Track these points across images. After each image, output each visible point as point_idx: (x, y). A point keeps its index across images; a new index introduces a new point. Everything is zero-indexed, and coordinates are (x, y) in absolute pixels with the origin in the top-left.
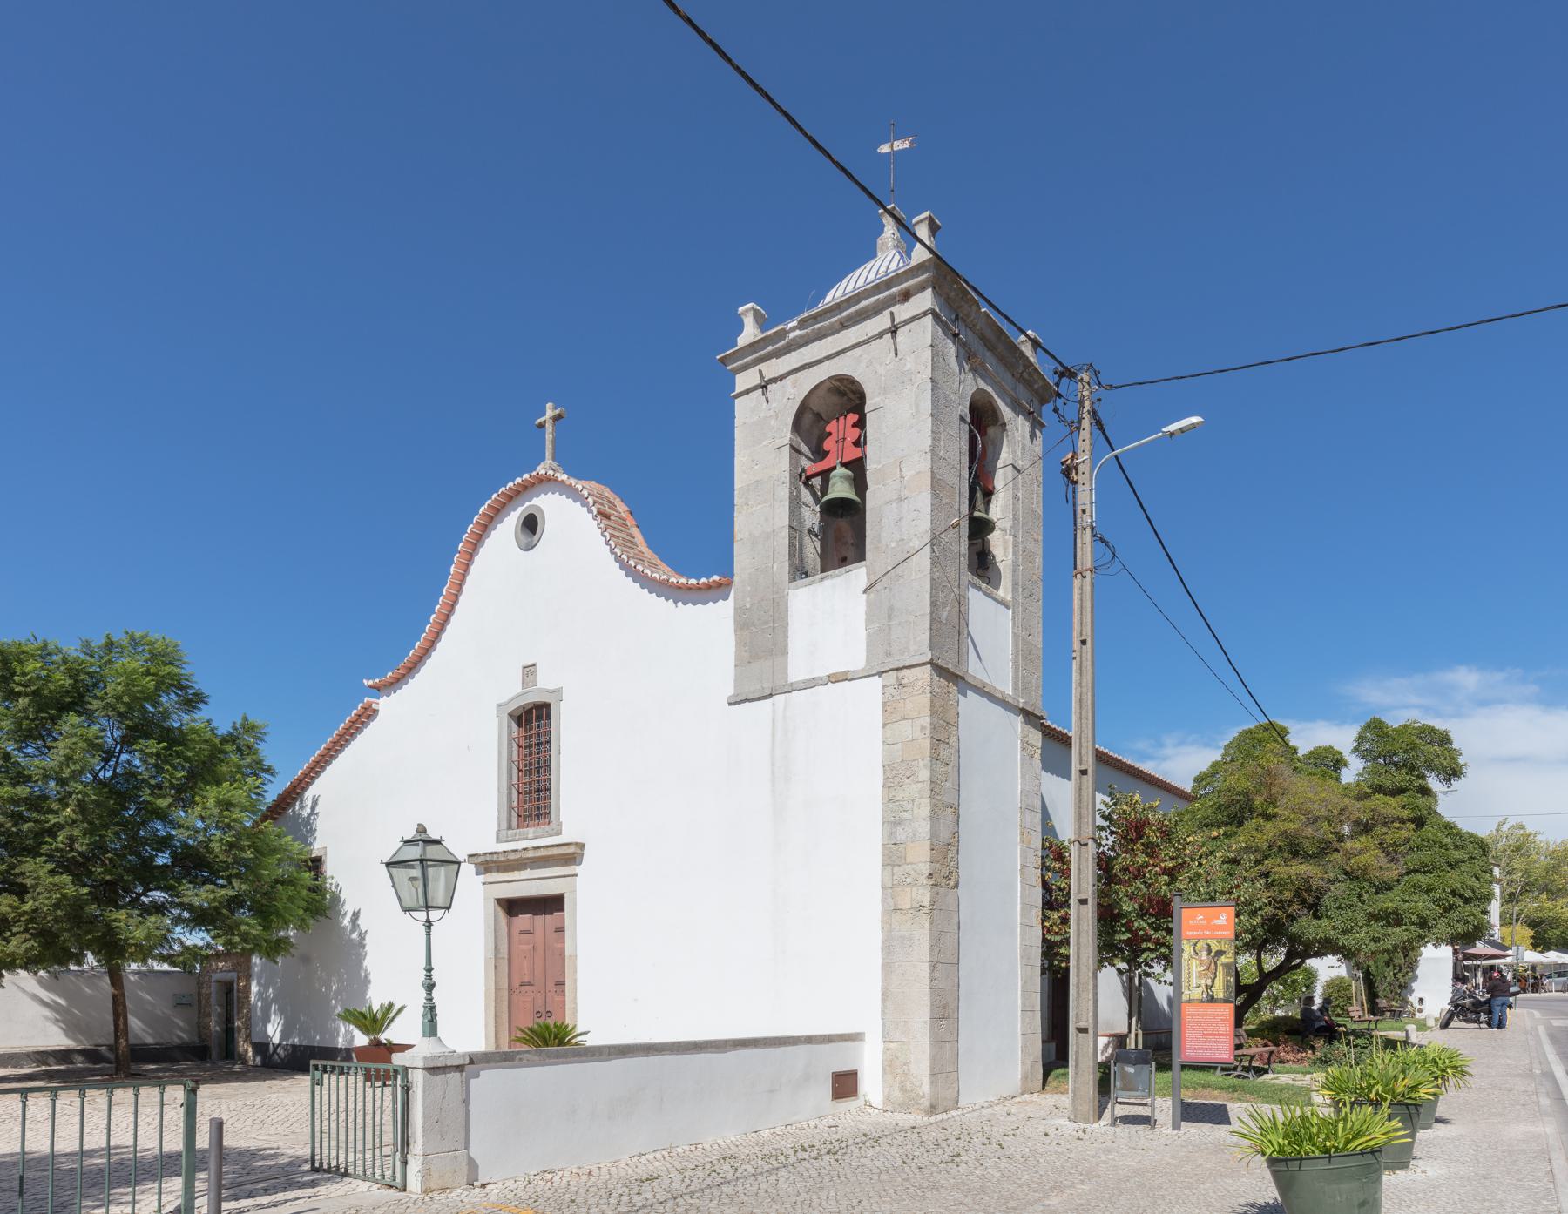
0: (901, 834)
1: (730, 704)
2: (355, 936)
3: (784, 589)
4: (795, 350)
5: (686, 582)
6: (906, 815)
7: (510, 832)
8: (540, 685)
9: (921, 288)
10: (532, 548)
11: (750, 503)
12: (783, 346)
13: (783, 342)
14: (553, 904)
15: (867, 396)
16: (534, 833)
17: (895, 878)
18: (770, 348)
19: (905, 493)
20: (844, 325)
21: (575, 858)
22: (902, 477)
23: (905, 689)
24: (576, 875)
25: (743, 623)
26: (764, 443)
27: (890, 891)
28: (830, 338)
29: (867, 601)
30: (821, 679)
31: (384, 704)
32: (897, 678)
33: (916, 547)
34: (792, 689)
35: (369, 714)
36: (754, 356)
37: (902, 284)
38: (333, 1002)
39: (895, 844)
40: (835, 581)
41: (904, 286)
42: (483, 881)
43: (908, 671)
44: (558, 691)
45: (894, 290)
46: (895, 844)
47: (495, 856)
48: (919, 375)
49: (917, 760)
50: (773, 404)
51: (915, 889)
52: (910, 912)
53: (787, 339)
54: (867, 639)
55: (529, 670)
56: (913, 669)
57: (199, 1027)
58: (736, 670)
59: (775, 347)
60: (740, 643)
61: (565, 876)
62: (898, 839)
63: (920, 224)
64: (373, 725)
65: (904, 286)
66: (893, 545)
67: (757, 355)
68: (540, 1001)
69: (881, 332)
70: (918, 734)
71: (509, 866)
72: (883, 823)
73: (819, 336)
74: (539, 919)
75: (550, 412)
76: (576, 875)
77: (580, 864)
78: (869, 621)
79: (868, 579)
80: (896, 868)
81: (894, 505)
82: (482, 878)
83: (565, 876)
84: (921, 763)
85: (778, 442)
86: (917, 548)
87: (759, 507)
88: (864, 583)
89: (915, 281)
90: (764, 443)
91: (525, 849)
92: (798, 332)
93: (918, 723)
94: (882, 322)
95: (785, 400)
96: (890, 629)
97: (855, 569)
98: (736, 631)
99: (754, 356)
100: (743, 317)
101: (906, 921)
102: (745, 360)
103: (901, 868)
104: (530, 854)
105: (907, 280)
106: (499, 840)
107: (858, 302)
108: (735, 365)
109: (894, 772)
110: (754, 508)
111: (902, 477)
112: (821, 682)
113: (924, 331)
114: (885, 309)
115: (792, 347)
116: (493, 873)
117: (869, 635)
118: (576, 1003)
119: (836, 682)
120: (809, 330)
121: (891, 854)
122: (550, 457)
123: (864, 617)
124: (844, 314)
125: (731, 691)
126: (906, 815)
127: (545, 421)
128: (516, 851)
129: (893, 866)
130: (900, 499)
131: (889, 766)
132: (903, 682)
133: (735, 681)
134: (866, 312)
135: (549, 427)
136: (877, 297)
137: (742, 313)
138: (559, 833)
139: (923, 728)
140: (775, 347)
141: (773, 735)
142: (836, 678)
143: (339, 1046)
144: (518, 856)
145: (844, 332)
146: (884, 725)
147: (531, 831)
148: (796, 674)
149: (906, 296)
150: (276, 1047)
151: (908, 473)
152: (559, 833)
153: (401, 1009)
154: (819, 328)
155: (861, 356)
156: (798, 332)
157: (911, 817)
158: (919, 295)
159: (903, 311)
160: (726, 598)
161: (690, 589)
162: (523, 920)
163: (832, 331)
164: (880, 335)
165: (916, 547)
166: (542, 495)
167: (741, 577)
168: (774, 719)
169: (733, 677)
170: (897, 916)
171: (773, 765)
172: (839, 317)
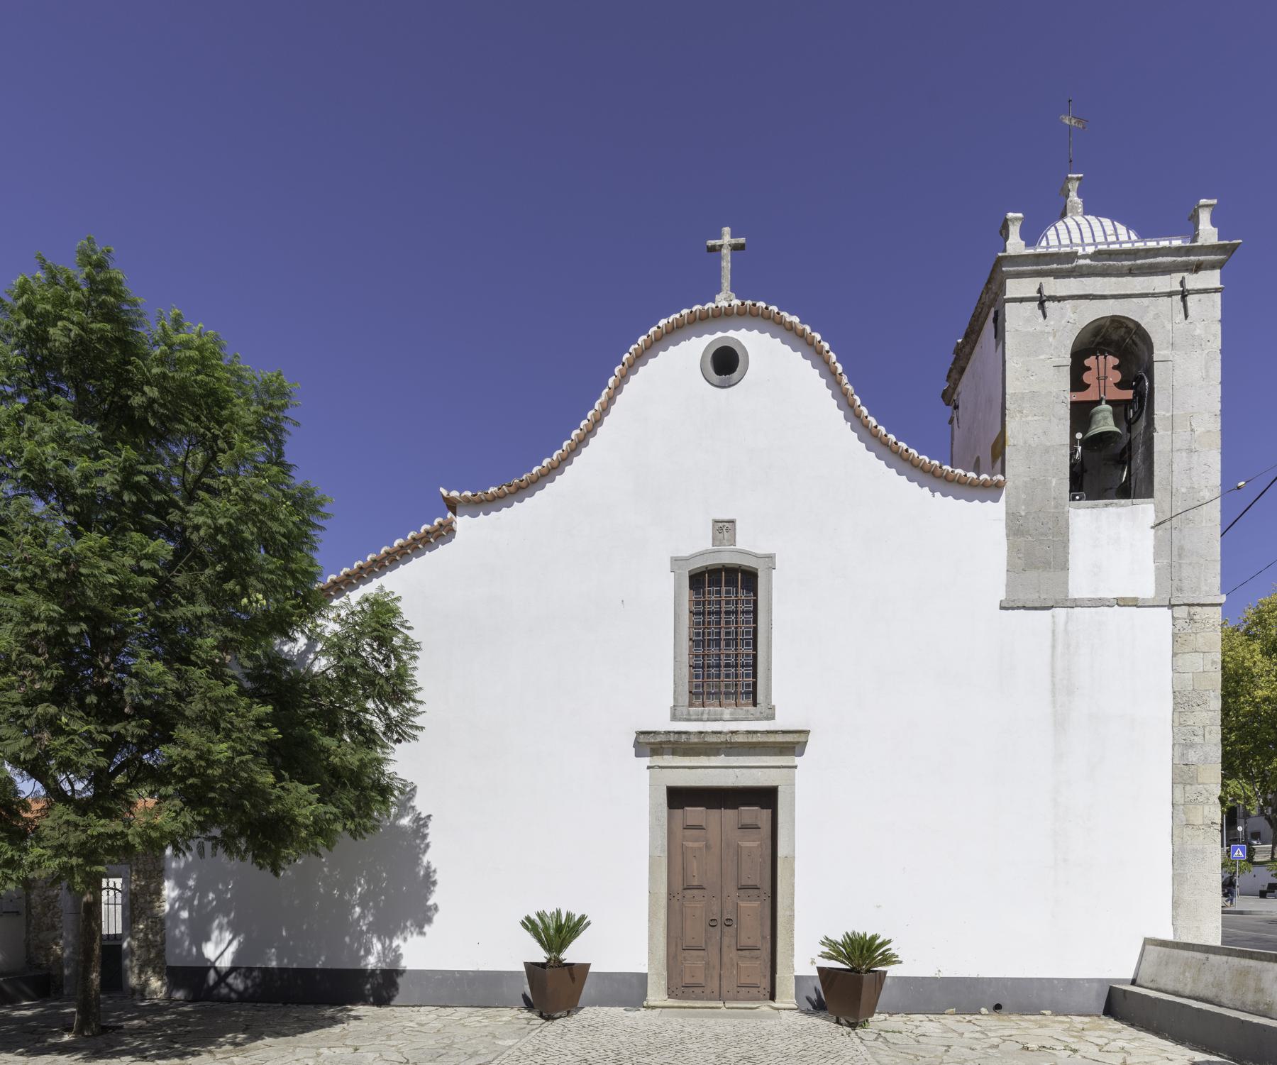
0: (1193, 756)
1: (1002, 608)
2: (405, 821)
3: (1064, 506)
4: (1075, 277)
5: (963, 473)
6: (1197, 739)
7: (692, 709)
8: (740, 545)
9: (1212, 266)
10: (730, 386)
11: (1025, 411)
12: (1067, 269)
13: (1070, 265)
14: (766, 797)
15: (1154, 345)
16: (731, 714)
17: (1187, 795)
18: (1055, 266)
19: (1195, 446)
20: (1131, 272)
21: (794, 747)
22: (1192, 430)
23: (1197, 625)
24: (796, 767)
25: (1015, 527)
26: (1042, 357)
27: (1182, 807)
28: (1113, 279)
29: (1156, 537)
30: (1109, 600)
31: (462, 523)
32: (1189, 613)
33: (1207, 498)
34: (1076, 604)
35: (445, 533)
36: (1035, 268)
37: (1201, 256)
38: (358, 910)
39: (1186, 765)
40: (1120, 510)
41: (1202, 258)
42: (649, 764)
43: (1200, 608)
44: (771, 557)
45: (1192, 258)
46: (1186, 765)
47: (684, 736)
48: (1209, 344)
49: (1208, 690)
50: (1051, 321)
51: (1207, 808)
52: (1201, 827)
53: (1074, 264)
54: (1155, 571)
55: (724, 528)
56: (1204, 608)
57: (28, 946)
58: (1007, 575)
59: (1059, 266)
60: (1013, 550)
61: (779, 767)
62: (1190, 760)
63: (1205, 208)
64: (442, 549)
65: (1202, 258)
66: (1184, 490)
67: (1039, 268)
68: (716, 909)
69: (1173, 292)
70: (1209, 667)
71: (692, 749)
72: (1174, 745)
73: (1105, 273)
74: (715, 814)
75: (727, 239)
76: (796, 767)
77: (801, 754)
78: (1157, 555)
79: (1156, 516)
80: (1188, 787)
81: (1184, 454)
82: (646, 761)
83: (779, 767)
84: (1212, 694)
85: (1057, 361)
86: (1207, 499)
87: (1036, 418)
88: (1152, 521)
89: (1213, 257)
90: (1042, 357)
91: (732, 732)
92: (1088, 261)
93: (1209, 657)
94: (1171, 282)
95: (1064, 322)
96: (1180, 567)
97: (1143, 503)
98: (1008, 536)
99: (1035, 268)
100: (1010, 223)
101: (1198, 836)
102: (1025, 268)
103: (1193, 788)
104: (740, 739)
105: (1206, 254)
106: (674, 717)
107: (1156, 256)
108: (1011, 269)
109: (1184, 699)
110: (1030, 418)
111: (1192, 430)
112: (1108, 604)
113: (1213, 306)
114: (1179, 271)
115: (1075, 274)
116: (665, 757)
117: (1157, 568)
118: (793, 910)
119: (1125, 606)
120: (1100, 264)
121: (1183, 774)
122: (729, 288)
123: (1152, 550)
124: (1139, 262)
125: (1002, 595)
126: (1197, 739)
127: (721, 246)
128: (720, 733)
129: (1185, 784)
130: (1190, 451)
131: (1180, 692)
132: (1195, 617)
133: (1007, 585)
134: (1157, 268)
135: (726, 252)
136: (1175, 259)
137: (1011, 220)
138: (771, 717)
139: (1214, 662)
140: (1059, 266)
141: (1054, 647)
142: (1122, 602)
143: (369, 967)
144: (722, 738)
145: (1129, 278)
146: (1174, 655)
147: (727, 712)
148: (1079, 586)
149: (1198, 268)
150: (223, 976)
151: (1199, 430)
152: (771, 717)
153: (901, 962)
154: (1110, 265)
155: (1148, 307)
156: (1088, 261)
157: (1202, 742)
158: (1208, 272)
159: (1194, 281)
160: (996, 500)
161: (952, 481)
162: (695, 814)
163: (1119, 273)
164: (1170, 294)
165: (1207, 498)
166: (768, 335)
167: (1014, 482)
168: (1053, 632)
169: (1005, 582)
170: (1189, 831)
171: (1053, 675)
172: (1133, 262)
